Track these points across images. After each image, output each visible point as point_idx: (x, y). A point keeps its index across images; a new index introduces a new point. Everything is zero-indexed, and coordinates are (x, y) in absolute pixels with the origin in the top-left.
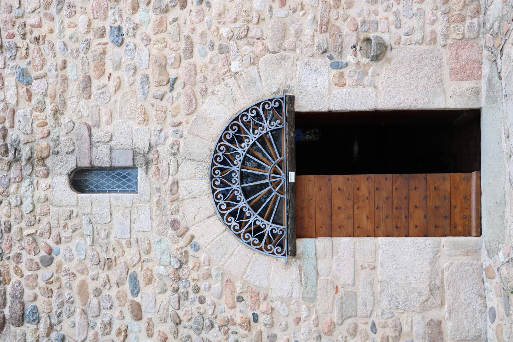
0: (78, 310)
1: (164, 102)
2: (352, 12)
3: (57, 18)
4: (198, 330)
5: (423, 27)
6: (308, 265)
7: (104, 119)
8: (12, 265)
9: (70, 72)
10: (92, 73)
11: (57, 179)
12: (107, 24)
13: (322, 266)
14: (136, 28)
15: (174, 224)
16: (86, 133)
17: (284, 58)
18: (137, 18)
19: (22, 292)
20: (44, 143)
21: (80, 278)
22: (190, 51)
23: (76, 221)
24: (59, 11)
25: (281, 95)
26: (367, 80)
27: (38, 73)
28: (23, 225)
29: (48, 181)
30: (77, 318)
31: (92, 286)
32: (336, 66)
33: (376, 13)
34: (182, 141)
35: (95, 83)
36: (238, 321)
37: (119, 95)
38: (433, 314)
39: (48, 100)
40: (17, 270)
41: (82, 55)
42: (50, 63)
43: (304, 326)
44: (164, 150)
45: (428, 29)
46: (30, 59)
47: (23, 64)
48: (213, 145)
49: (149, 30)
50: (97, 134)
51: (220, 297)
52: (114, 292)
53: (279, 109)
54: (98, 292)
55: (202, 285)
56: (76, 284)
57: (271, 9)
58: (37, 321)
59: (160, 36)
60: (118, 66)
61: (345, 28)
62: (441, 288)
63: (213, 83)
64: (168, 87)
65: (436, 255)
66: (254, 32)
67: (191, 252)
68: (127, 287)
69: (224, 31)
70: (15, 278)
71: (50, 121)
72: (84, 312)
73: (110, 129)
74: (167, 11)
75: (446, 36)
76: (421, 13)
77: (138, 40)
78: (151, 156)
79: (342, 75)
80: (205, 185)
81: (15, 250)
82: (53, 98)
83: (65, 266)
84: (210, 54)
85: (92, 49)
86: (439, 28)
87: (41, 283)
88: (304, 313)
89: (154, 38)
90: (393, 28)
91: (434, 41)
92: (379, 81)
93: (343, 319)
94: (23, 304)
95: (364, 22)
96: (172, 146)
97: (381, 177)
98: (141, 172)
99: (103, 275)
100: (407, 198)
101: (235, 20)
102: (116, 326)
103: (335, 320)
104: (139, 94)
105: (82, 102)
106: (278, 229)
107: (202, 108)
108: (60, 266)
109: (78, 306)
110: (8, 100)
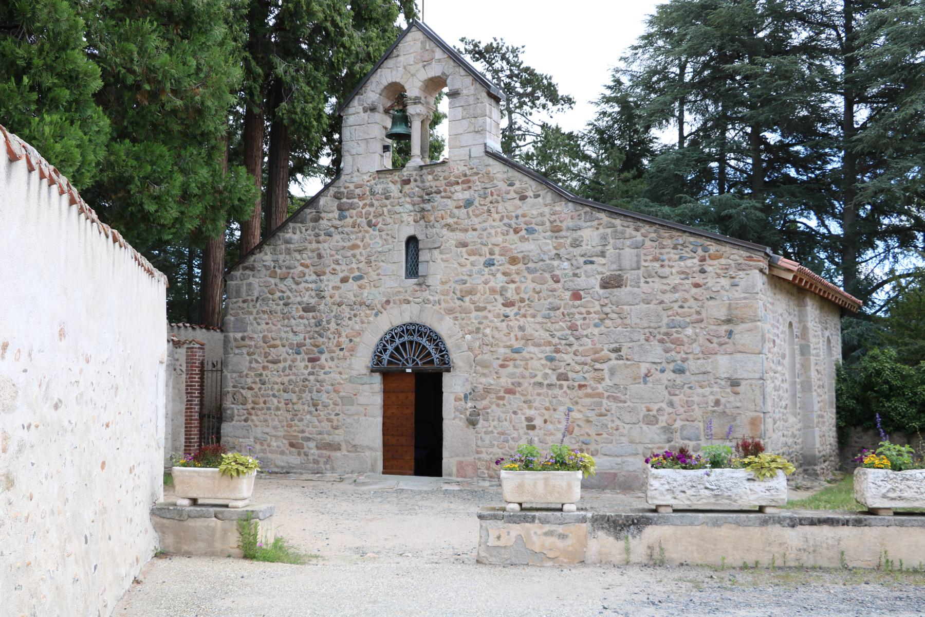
0: (345, 244)
1: (452, 294)
2: (494, 407)
3: (501, 224)
4: (335, 317)
5: (484, 447)
6: (366, 379)
7: (444, 256)
8: (368, 202)
9: (471, 233)
10: (469, 247)
11: (412, 228)
12: (496, 257)
13: (367, 387)
14: (494, 275)
15: (388, 302)
16: (436, 246)
17: (471, 366)
18: (499, 275)
19: (354, 209)
20: (432, 218)
21: (361, 244)
22: (479, 309)
23: (390, 242)
24: (505, 224)
25: (452, 364)
26: (458, 414)
27: (471, 213)
28: (389, 207)
29: (412, 223)
30: (341, 244)
31: (357, 252)
32: (466, 397)
33: (493, 420)
34: (430, 305)
35: (464, 249)
36: (340, 339)
37: (456, 266)
38: (344, 446)
39: (455, 220)
40: (365, 205)
41: (479, 241)
42: (476, 220)
43: (337, 376)
44: (426, 295)
45: (484, 450)
46: (480, 207)
47: (476, 203)
48: (428, 325)
49: (492, 284)
50: (436, 252)
51: (352, 329)
52: (354, 266)
53: (445, 364)
54: (354, 256)
55: (357, 319)
56: (358, 242)
57: (498, 359)
58: (340, 220)
59: (488, 290)
60: (473, 264)
61: (485, 402)
62: (356, 451)
63: (460, 324)
64: (459, 296)
65: (371, 449)
66: (486, 349)
67: (374, 312)
68: (357, 274)
69: (488, 331)
70: (361, 204)
71: (444, 222)
72: (344, 248)
73: (439, 261)
74: (501, 295)
75: (479, 459)
76: (492, 446)
77: (487, 276)
78: (424, 286)
79: (461, 400)
80: (407, 320)
81: (376, 203)
82: (456, 223)
83: (367, 235)
84: (476, 322)
85: (483, 248)
86: (484, 456)
87: (359, 220)
88: (344, 376)
89: (487, 286)
90: (484, 430)
91: (478, 453)
92: (457, 421)
93: (341, 398)
94: (348, 210)
95: (488, 413)
96: (428, 300)
97: (413, 421)
98: (415, 281)
99: (363, 259)
100: (402, 435)
101: (493, 337)
102: (337, 267)
103: (341, 394)
104: (456, 278)
105: (454, 242)
106: (385, 362)
107: (447, 318)
108: (367, 232)
109: (348, 244)
110: (456, 194)
